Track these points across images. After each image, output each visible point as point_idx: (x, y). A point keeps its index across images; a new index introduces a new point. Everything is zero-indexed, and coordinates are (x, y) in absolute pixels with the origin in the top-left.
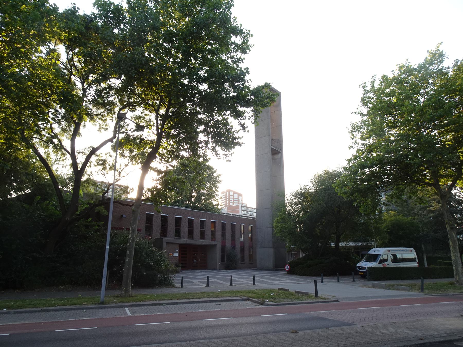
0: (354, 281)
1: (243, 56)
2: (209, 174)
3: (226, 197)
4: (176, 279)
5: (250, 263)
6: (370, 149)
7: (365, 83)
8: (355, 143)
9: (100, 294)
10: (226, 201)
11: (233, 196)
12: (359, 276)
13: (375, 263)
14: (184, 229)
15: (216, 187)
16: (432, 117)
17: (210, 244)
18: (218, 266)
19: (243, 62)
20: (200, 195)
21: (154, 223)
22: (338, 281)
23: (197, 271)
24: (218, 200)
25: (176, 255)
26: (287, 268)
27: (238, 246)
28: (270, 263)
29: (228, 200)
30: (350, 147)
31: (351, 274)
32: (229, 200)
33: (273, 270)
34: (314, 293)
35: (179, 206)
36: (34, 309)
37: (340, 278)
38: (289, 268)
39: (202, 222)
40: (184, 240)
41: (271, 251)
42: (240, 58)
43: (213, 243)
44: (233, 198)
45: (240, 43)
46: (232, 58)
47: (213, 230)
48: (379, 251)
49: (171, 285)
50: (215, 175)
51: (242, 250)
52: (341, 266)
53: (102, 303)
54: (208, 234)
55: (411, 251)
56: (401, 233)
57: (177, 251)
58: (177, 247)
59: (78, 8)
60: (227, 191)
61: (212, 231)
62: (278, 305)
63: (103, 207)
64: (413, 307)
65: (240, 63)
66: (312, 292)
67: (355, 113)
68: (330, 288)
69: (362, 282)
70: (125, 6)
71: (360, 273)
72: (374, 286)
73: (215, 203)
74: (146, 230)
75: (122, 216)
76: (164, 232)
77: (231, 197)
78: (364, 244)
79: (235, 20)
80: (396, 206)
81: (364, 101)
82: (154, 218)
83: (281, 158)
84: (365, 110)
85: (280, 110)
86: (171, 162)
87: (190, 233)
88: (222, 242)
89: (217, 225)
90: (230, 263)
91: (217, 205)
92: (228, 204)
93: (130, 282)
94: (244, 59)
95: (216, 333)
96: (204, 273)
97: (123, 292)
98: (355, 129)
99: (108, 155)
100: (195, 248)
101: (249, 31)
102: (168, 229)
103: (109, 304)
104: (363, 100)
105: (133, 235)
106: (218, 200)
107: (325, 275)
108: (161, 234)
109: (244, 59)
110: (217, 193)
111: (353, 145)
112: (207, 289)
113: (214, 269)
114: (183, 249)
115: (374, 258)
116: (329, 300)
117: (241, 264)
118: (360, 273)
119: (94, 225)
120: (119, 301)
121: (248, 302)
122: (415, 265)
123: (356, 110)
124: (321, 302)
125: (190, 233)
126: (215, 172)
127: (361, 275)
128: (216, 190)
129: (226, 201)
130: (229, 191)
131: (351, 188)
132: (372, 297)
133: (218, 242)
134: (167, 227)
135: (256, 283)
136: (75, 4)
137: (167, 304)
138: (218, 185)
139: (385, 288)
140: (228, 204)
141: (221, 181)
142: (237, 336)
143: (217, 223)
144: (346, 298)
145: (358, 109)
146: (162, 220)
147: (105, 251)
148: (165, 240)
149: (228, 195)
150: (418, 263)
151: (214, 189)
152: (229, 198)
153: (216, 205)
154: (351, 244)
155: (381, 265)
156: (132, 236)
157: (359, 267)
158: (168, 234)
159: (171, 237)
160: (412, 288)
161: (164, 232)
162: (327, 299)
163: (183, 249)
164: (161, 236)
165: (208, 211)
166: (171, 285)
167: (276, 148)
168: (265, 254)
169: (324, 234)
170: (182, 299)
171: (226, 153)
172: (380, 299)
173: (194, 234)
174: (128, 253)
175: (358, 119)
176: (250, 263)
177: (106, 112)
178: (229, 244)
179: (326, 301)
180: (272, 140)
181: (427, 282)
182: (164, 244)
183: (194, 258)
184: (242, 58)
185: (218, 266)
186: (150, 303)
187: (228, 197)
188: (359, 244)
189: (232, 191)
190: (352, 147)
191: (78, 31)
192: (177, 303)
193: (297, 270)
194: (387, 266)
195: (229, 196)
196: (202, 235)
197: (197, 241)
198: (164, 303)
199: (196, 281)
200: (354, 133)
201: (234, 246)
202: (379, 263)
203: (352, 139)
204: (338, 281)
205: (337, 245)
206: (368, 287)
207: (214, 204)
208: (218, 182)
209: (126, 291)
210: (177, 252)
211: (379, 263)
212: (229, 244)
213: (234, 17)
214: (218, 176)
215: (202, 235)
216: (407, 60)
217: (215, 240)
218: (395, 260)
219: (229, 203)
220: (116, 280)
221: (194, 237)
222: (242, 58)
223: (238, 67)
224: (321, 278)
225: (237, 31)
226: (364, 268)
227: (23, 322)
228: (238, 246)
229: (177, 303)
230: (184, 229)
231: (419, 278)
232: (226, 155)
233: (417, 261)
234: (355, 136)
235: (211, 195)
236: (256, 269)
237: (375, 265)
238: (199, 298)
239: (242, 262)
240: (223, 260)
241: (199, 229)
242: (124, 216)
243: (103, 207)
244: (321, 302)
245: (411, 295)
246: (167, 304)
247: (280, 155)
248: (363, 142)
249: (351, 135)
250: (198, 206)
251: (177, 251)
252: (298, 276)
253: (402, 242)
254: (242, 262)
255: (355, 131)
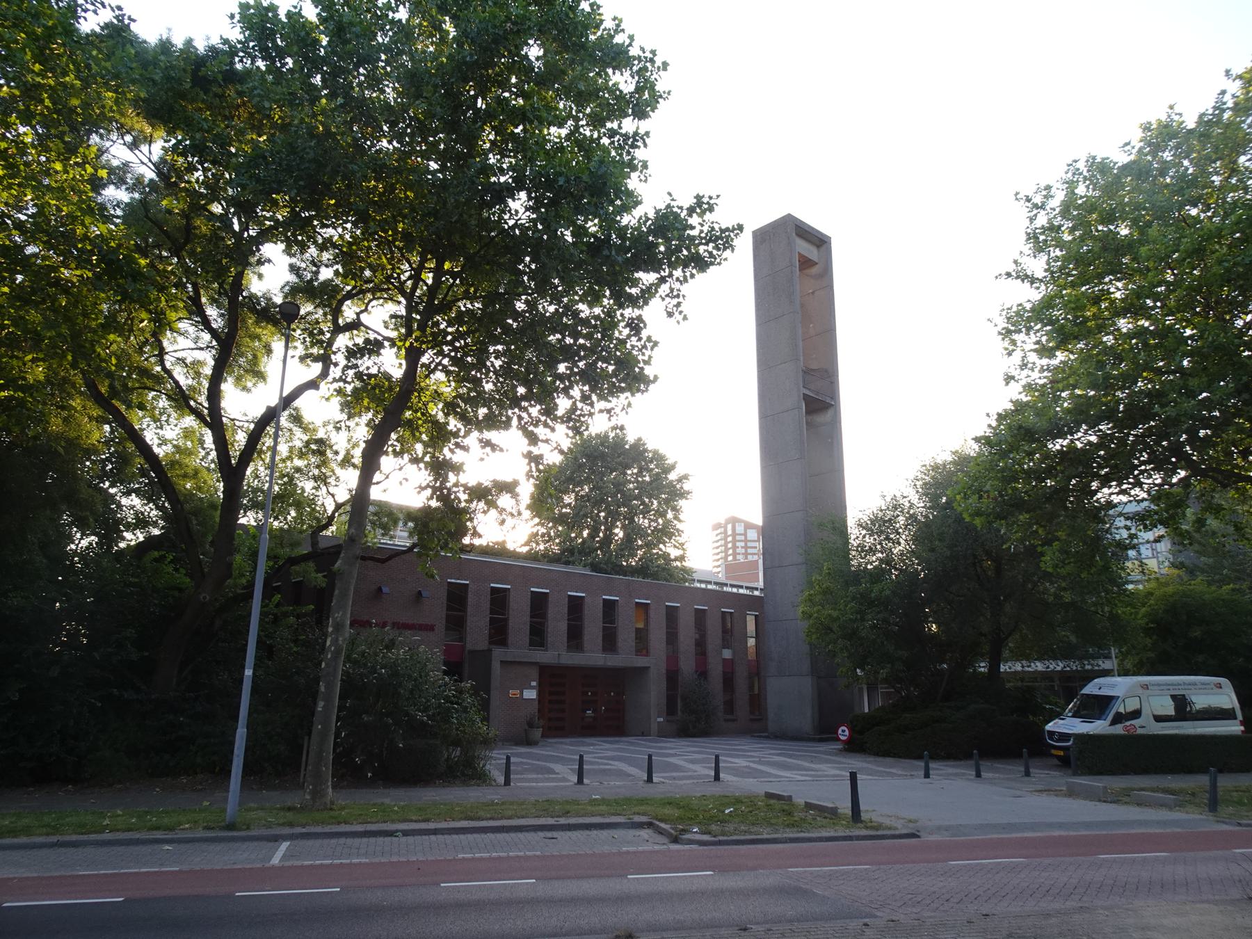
0: (1027, 774)
1: (644, 126)
2: (658, 474)
3: (725, 538)
4: (493, 762)
5: (752, 720)
6: (1061, 378)
7: (1048, 188)
8: (1024, 366)
9: (226, 800)
10: (727, 550)
11: (745, 535)
12: (1056, 762)
13: (1099, 722)
14: (557, 625)
15: (674, 509)
16: (1228, 270)
17: (629, 665)
18: (654, 727)
19: (645, 145)
20: (633, 532)
21: (469, 609)
22: (978, 775)
23: (588, 740)
24: (682, 544)
25: (530, 694)
26: (844, 733)
27: (716, 671)
28: (805, 719)
29: (730, 545)
30: (1009, 379)
31: (1020, 756)
32: (735, 547)
33: (813, 740)
34: (850, 805)
35: (573, 563)
36: (423, 826)
37: (932, 765)
38: (847, 733)
39: (609, 606)
40: (556, 653)
41: (806, 685)
42: (636, 134)
43: (640, 662)
44: (746, 541)
45: (632, 88)
46: (612, 133)
47: (641, 625)
48: (1113, 686)
49: (479, 777)
50: (672, 476)
51: (728, 681)
52: (1002, 733)
53: (231, 827)
54: (626, 638)
55: (1219, 686)
56: (1197, 633)
57: (534, 684)
58: (534, 672)
59: (130, 18)
60: (728, 522)
61: (638, 630)
62: (720, 843)
63: (311, 565)
64: (1134, 860)
65: (638, 147)
66: (845, 807)
67: (1009, 275)
68: (900, 793)
69: (1062, 779)
70: (311, 13)
71: (1054, 752)
72: (1072, 793)
73: (674, 553)
74: (447, 629)
75: (380, 589)
76: (499, 633)
77: (738, 538)
78: (1074, 666)
79: (618, 26)
80: (1197, 552)
81: (1037, 241)
82: (470, 595)
83: (835, 424)
84: (1037, 266)
85: (829, 287)
86: (464, 437)
87: (575, 636)
88: (668, 658)
89: (652, 613)
90: (693, 717)
91: (682, 558)
92: (730, 558)
93: (327, 770)
94: (647, 134)
95: (664, 915)
96: (608, 746)
97: (308, 797)
98: (1019, 321)
99: (330, 427)
100: (591, 675)
101: (653, 52)
102: (511, 623)
103: (248, 828)
104: (1032, 237)
105: (337, 640)
106: (682, 544)
107: (935, 757)
108: (491, 636)
109: (647, 134)
110: (679, 526)
111: (1014, 373)
112: (649, 791)
113: (643, 734)
114: (551, 678)
115: (1097, 706)
116: (897, 832)
117: (726, 720)
118: (1054, 752)
119: (286, 615)
120: (281, 821)
121: (645, 833)
122: (1234, 728)
123: (1011, 268)
124: (859, 838)
125: (575, 636)
126: (673, 467)
127: (1058, 757)
128: (676, 518)
129: (727, 550)
130: (734, 521)
131: (995, 499)
132: (1033, 827)
133: (656, 661)
134: (506, 620)
135: (722, 775)
136: (120, 8)
137: (406, 833)
138: (682, 503)
139: (1090, 795)
140: (730, 558)
141: (688, 493)
142: (791, 921)
143: (652, 607)
144: (947, 828)
145: (1016, 262)
146: (493, 602)
147: (241, 681)
148: (498, 653)
149: (730, 532)
150: (1242, 723)
151: (670, 515)
152: (734, 541)
153: (676, 559)
154: (1039, 666)
155: (1119, 729)
156: (335, 641)
157: (1051, 733)
158: (512, 638)
159: (519, 646)
160: (1183, 800)
161: (499, 633)
162: (890, 828)
163: (551, 678)
164: (490, 643)
165: (655, 576)
166: (479, 777)
167: (817, 393)
168: (790, 693)
169: (946, 641)
170: (461, 819)
171: (609, 406)
172: (1056, 833)
173: (586, 638)
174: (322, 689)
175: (1030, 295)
176: (752, 720)
177: (321, 312)
178: (687, 665)
179: (879, 834)
180: (807, 372)
181: (1226, 782)
182: (496, 666)
183: (586, 705)
184: (642, 131)
185: (654, 727)
186: (360, 828)
187: (730, 539)
188: (1058, 666)
189: (740, 521)
190: (1013, 378)
191: (180, 89)
192: (435, 832)
193: (877, 738)
194: (1140, 731)
195: (734, 534)
196: (610, 641)
197: (593, 656)
198: (397, 831)
199: (549, 771)
200: (1015, 337)
201: (702, 673)
202: (1113, 723)
203: (1010, 354)
204: (978, 775)
205: (994, 667)
206: (1057, 793)
207: (672, 557)
208: (683, 495)
209: (317, 794)
210: (533, 688)
211: (1113, 723)
212: (687, 665)
213: (615, 19)
214: (680, 480)
215: (610, 641)
216: (1171, 107)
217: (647, 655)
218: (1183, 709)
219: (735, 554)
220: (276, 765)
221: (586, 645)
222: (642, 131)
223: (633, 158)
224: (922, 764)
225: (618, 57)
226: (1064, 737)
227: (1019, 835)
228: (716, 671)
229: (435, 832)
230: (557, 625)
231: (1203, 771)
232: (609, 411)
233: (1240, 717)
234: (1019, 344)
235: (666, 532)
236: (767, 737)
237: (1099, 727)
238: (510, 818)
239: (729, 717)
240: (671, 710)
241: (601, 624)
242: (385, 590)
243: (311, 564)
244: (859, 838)
245: (1164, 823)
246: (406, 833)
247: (830, 412)
248: (1045, 361)
249: (1006, 343)
250: (629, 566)
251: (534, 684)
252: (871, 759)
253: (1200, 658)
254: (729, 717)
255: (1020, 331)
